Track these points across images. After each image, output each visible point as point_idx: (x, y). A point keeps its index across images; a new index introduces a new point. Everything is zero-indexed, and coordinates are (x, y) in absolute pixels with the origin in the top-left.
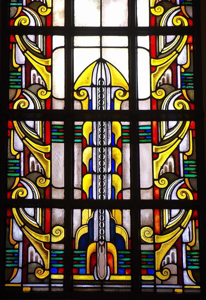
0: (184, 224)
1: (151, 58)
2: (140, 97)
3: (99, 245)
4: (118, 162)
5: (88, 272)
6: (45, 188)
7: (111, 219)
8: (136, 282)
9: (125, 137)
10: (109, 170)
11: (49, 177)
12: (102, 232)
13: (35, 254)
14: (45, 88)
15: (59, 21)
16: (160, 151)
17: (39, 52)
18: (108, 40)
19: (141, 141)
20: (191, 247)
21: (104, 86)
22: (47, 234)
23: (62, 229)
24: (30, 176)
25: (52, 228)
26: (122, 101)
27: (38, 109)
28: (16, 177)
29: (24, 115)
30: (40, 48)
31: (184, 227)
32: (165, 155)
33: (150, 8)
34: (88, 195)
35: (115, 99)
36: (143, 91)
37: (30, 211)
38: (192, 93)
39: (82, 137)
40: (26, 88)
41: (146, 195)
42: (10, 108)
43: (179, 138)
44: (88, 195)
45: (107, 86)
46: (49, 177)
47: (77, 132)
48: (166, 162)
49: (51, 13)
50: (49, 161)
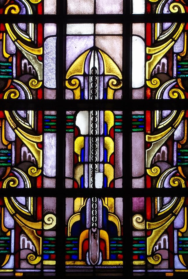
0: (176, 36)
3: (92, 232)
4: (111, 151)
6: (36, 5)
7: (103, 207)
9: (117, 127)
10: (102, 159)
11: (41, 166)
13: (26, 242)
16: (152, 140)
18: (103, 28)
19: (134, 130)
21: (97, 163)
23: (55, 218)
25: (44, 216)
26: (115, 90)
30: (31, 125)
31: (175, 39)
32: (159, 54)
33: (146, 80)
34: (79, 183)
36: (138, 79)
37: (22, 200)
41: (138, 184)
44: (79, 183)
45: (99, 75)
46: (41, 167)
48: (159, 63)
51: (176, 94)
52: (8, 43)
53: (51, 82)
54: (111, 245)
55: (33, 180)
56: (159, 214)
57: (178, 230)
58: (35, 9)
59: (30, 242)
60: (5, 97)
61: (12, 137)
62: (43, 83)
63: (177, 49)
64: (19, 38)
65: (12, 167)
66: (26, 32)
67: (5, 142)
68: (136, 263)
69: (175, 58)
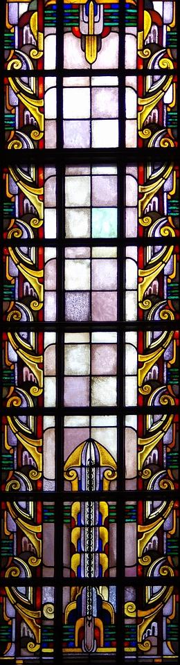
1: (138, 437)
2: (127, 117)
3: (87, 620)
5: (77, 645)
8: (121, 653)
11: (42, 300)
12: (89, 607)
14: (37, 385)
15: (50, 64)
17: (31, 263)
18: (98, 420)
20: (171, 108)
26: (111, 481)
28: (9, 470)
29: (18, 496)
32: (150, 277)
35: (105, 480)
38: (175, 52)
39: (70, 517)
41: (130, 573)
42: (4, 319)
43: (164, 178)
47: (66, 519)
51: (166, 485)
52: (11, 267)
53: (50, 472)
55: (34, 483)
57: (167, 532)
58: (35, 66)
59: (29, 630)
60: (7, 576)
62: (43, 474)
63: (166, 440)
65: (14, 470)
67: (9, 108)
68: (127, 649)
69: (165, 366)
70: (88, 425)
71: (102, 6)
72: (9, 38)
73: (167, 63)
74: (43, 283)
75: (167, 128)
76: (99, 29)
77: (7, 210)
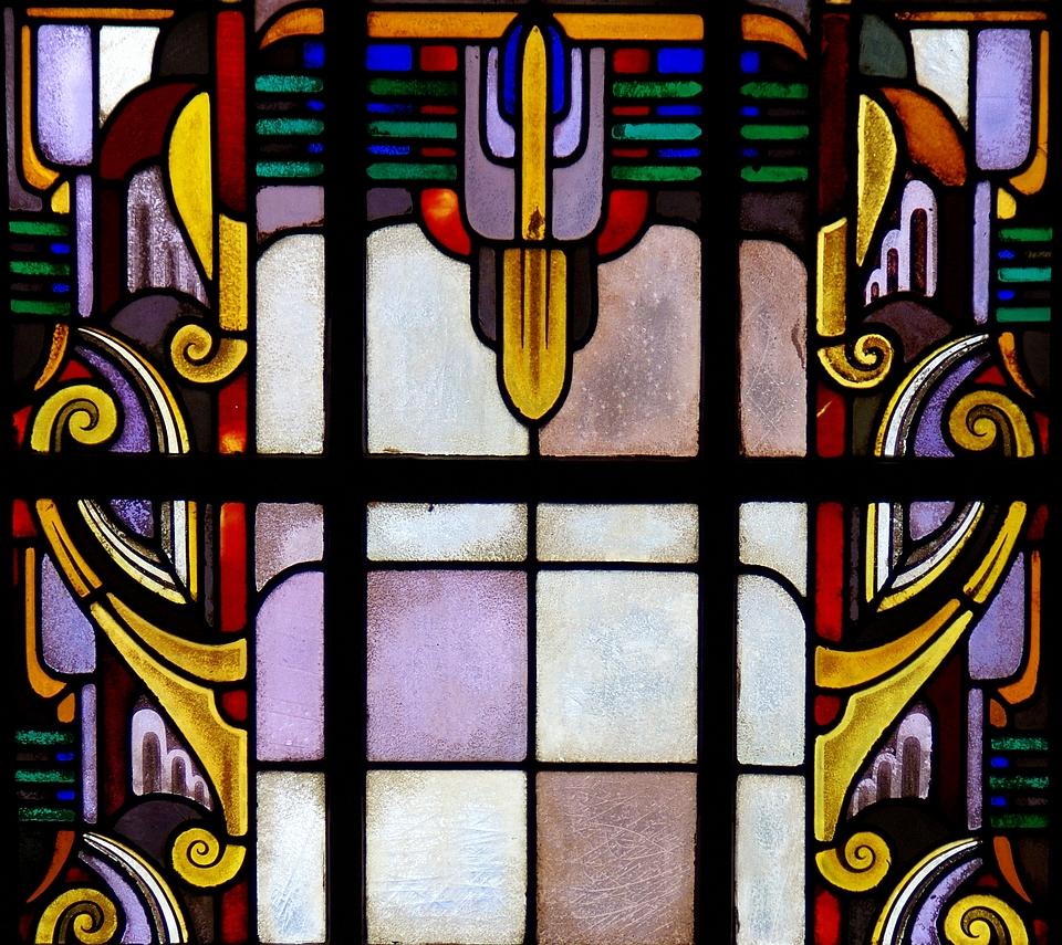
0: (980, 582)
11: (243, 830)
14: (215, 821)
15: (290, 418)
18: (576, 527)
22: (235, 638)
24: (131, 819)
25: (256, 600)
27: (174, 449)
32: (887, 691)
33: (812, 846)
40: (101, 319)
48: (887, 738)
49: (249, 366)
50: (243, 734)
51: (987, 428)
52: (48, 609)
54: (632, 131)
56: (888, 603)
61: (84, 660)
64: (116, 582)
66: (155, 544)
67: (42, 176)
70: (520, 555)
71: (598, 57)
72: (37, 248)
73: (989, 424)
74: (248, 721)
75: (994, 328)
76: (578, 213)
77: (32, 777)
